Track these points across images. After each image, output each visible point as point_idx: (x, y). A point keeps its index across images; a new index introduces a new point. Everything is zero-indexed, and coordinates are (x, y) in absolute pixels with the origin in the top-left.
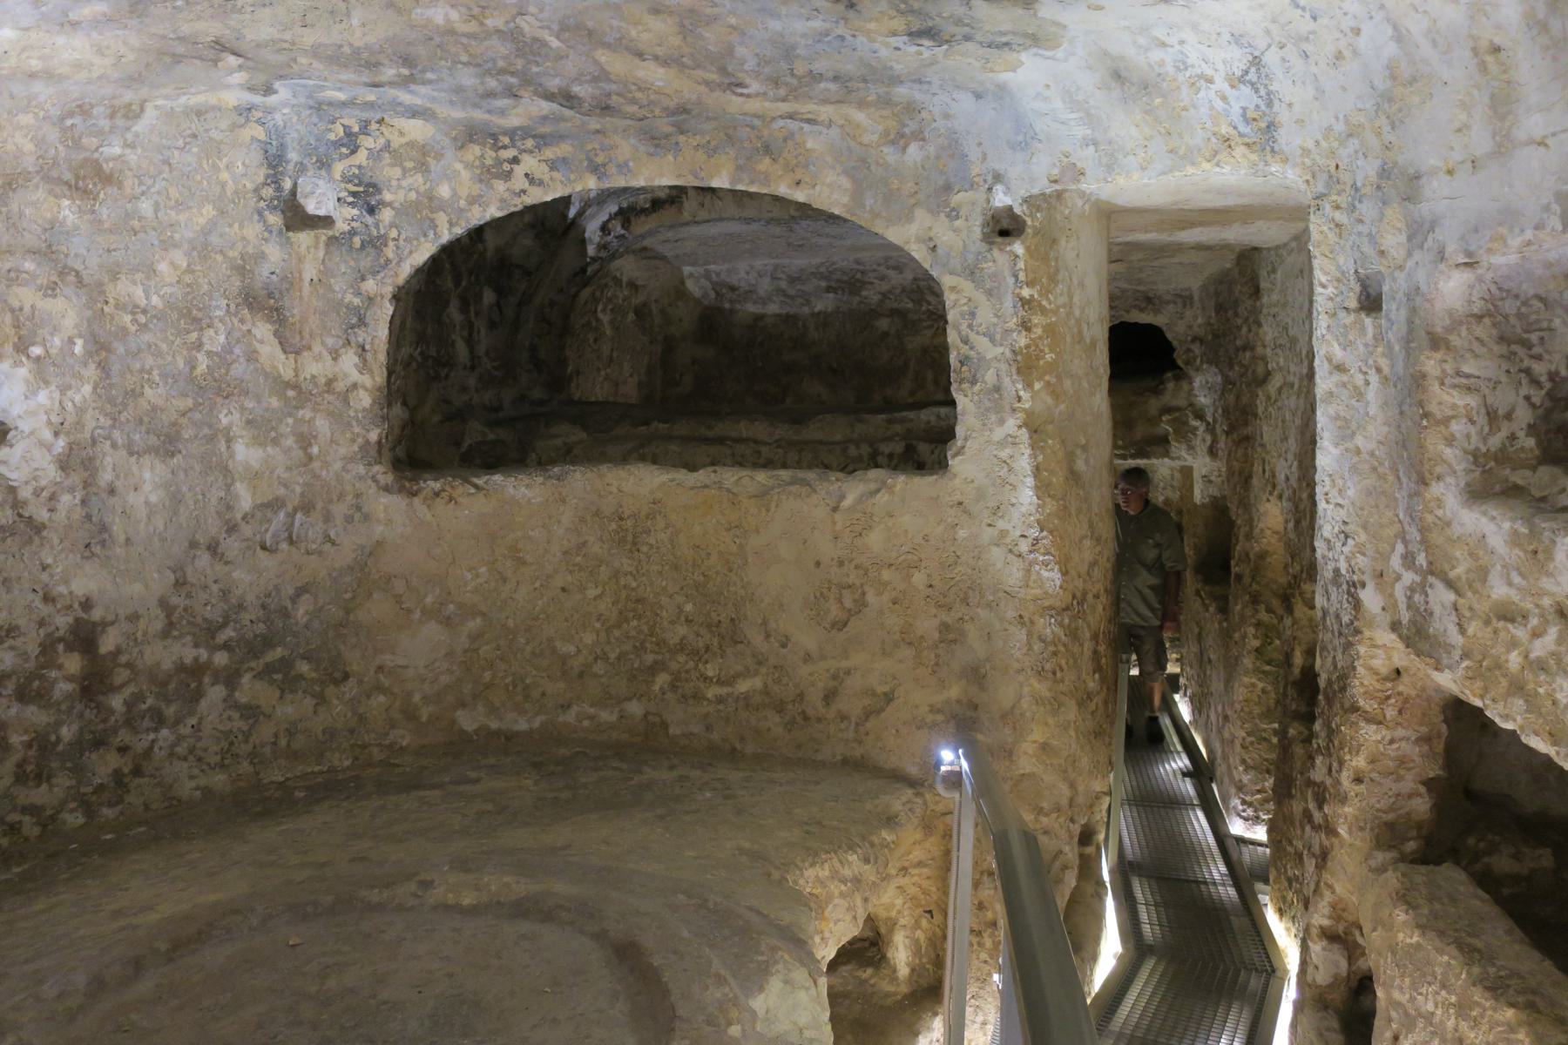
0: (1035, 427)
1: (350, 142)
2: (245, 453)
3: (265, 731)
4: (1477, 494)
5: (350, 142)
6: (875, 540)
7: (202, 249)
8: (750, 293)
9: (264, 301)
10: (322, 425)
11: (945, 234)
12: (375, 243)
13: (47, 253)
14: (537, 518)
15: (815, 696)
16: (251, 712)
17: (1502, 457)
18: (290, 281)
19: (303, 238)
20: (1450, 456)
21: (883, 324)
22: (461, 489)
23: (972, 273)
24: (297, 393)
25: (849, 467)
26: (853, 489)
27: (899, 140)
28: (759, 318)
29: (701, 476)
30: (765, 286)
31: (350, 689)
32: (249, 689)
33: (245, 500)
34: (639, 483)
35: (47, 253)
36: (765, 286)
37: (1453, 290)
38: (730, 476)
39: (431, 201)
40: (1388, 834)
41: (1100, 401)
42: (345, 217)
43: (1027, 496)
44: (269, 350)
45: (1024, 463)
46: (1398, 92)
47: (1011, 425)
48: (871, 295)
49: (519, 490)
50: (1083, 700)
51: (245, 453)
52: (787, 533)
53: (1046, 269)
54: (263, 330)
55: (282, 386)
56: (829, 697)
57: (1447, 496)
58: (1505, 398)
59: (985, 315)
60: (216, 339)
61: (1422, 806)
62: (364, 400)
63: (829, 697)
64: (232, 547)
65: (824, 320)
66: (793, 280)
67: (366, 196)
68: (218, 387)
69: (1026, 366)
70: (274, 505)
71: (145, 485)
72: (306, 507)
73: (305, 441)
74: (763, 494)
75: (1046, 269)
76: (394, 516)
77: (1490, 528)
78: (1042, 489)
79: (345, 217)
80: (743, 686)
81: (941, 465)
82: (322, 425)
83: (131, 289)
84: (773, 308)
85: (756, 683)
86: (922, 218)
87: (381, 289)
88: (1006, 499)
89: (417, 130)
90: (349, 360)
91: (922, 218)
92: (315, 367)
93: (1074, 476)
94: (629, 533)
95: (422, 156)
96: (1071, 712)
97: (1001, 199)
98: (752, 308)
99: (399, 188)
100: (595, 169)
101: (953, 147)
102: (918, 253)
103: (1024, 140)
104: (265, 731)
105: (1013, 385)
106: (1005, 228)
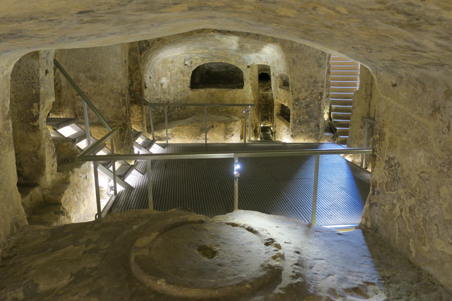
0: (251, 84)
1: (192, 58)
2: (179, 86)
3: (180, 113)
4: (279, 88)
5: (192, 58)
6: (236, 95)
7: (178, 68)
8: (213, 69)
9: (182, 72)
10: (185, 84)
11: (243, 67)
12: (191, 67)
13: (169, 69)
14: (203, 93)
15: (230, 111)
16: (179, 111)
17: (281, 85)
18: (184, 70)
19: (186, 66)
20: (278, 85)
21: (231, 73)
22: (196, 90)
23: (246, 71)
24: (183, 81)
25: (234, 88)
26: (234, 90)
27: (240, 59)
28: (215, 72)
29: (219, 89)
30: (215, 67)
31: (186, 110)
32: (179, 109)
33: (179, 91)
34: (213, 90)
35: (169, 69)
36: (215, 67)
37: (277, 74)
38: (222, 89)
39: (197, 63)
40: (277, 115)
41: (257, 82)
42: (189, 64)
43: (250, 91)
44: (182, 77)
45: (250, 88)
46: (273, 62)
47: (249, 84)
48: (230, 69)
49: (202, 91)
50: (256, 110)
51: (179, 86)
52: (230, 95)
53: (252, 70)
54: (182, 75)
55: (182, 80)
56: (232, 111)
57: (278, 88)
58: (281, 81)
59: (247, 74)
60: (178, 76)
61: (279, 112)
62: (189, 81)
63: (232, 111)
64: (178, 95)
65: (223, 72)
66: (219, 67)
67: (191, 63)
68: (177, 80)
69: (250, 79)
70: (181, 91)
71: (172, 88)
72: (183, 92)
73: (184, 85)
74: (225, 91)
75: (252, 70)
76: (192, 93)
77: (279, 89)
78: (252, 90)
79: (189, 64)
80: (223, 110)
81: (243, 88)
82: (185, 84)
83: (173, 71)
84: (217, 70)
85: (224, 110)
86: (241, 66)
87: (191, 71)
88: (249, 92)
89: (197, 57)
90: (188, 77)
91: (241, 66)
92: (185, 78)
93: (255, 89)
94: (212, 95)
95: (197, 59)
96: (254, 111)
97: (248, 64)
98: (214, 70)
99: (194, 62)
100: (212, 60)
101: (244, 60)
102: (241, 69)
103: (250, 60)
104: (180, 113)
105: (249, 81)
106: (249, 67)
